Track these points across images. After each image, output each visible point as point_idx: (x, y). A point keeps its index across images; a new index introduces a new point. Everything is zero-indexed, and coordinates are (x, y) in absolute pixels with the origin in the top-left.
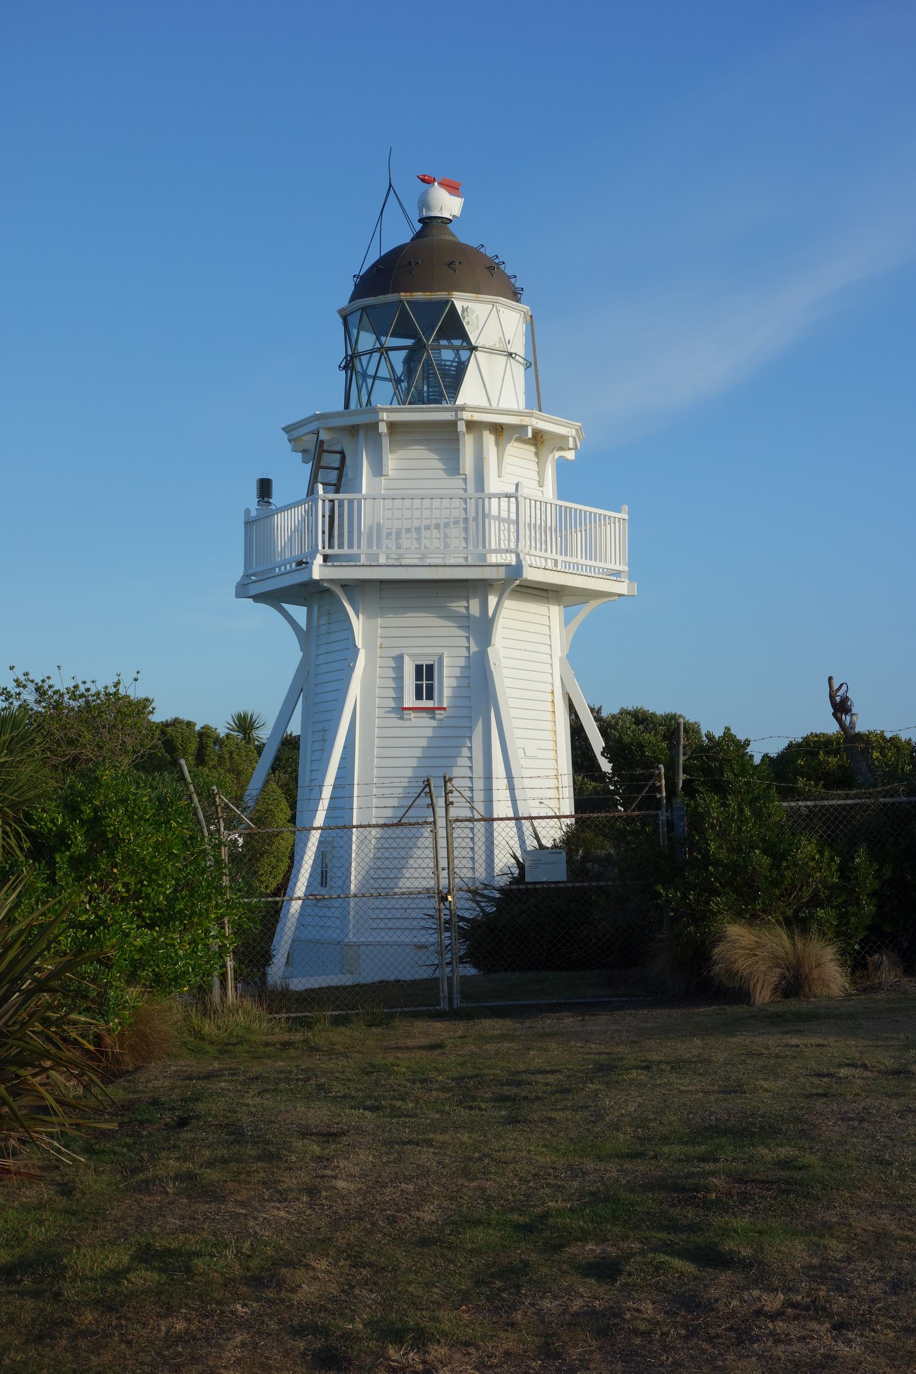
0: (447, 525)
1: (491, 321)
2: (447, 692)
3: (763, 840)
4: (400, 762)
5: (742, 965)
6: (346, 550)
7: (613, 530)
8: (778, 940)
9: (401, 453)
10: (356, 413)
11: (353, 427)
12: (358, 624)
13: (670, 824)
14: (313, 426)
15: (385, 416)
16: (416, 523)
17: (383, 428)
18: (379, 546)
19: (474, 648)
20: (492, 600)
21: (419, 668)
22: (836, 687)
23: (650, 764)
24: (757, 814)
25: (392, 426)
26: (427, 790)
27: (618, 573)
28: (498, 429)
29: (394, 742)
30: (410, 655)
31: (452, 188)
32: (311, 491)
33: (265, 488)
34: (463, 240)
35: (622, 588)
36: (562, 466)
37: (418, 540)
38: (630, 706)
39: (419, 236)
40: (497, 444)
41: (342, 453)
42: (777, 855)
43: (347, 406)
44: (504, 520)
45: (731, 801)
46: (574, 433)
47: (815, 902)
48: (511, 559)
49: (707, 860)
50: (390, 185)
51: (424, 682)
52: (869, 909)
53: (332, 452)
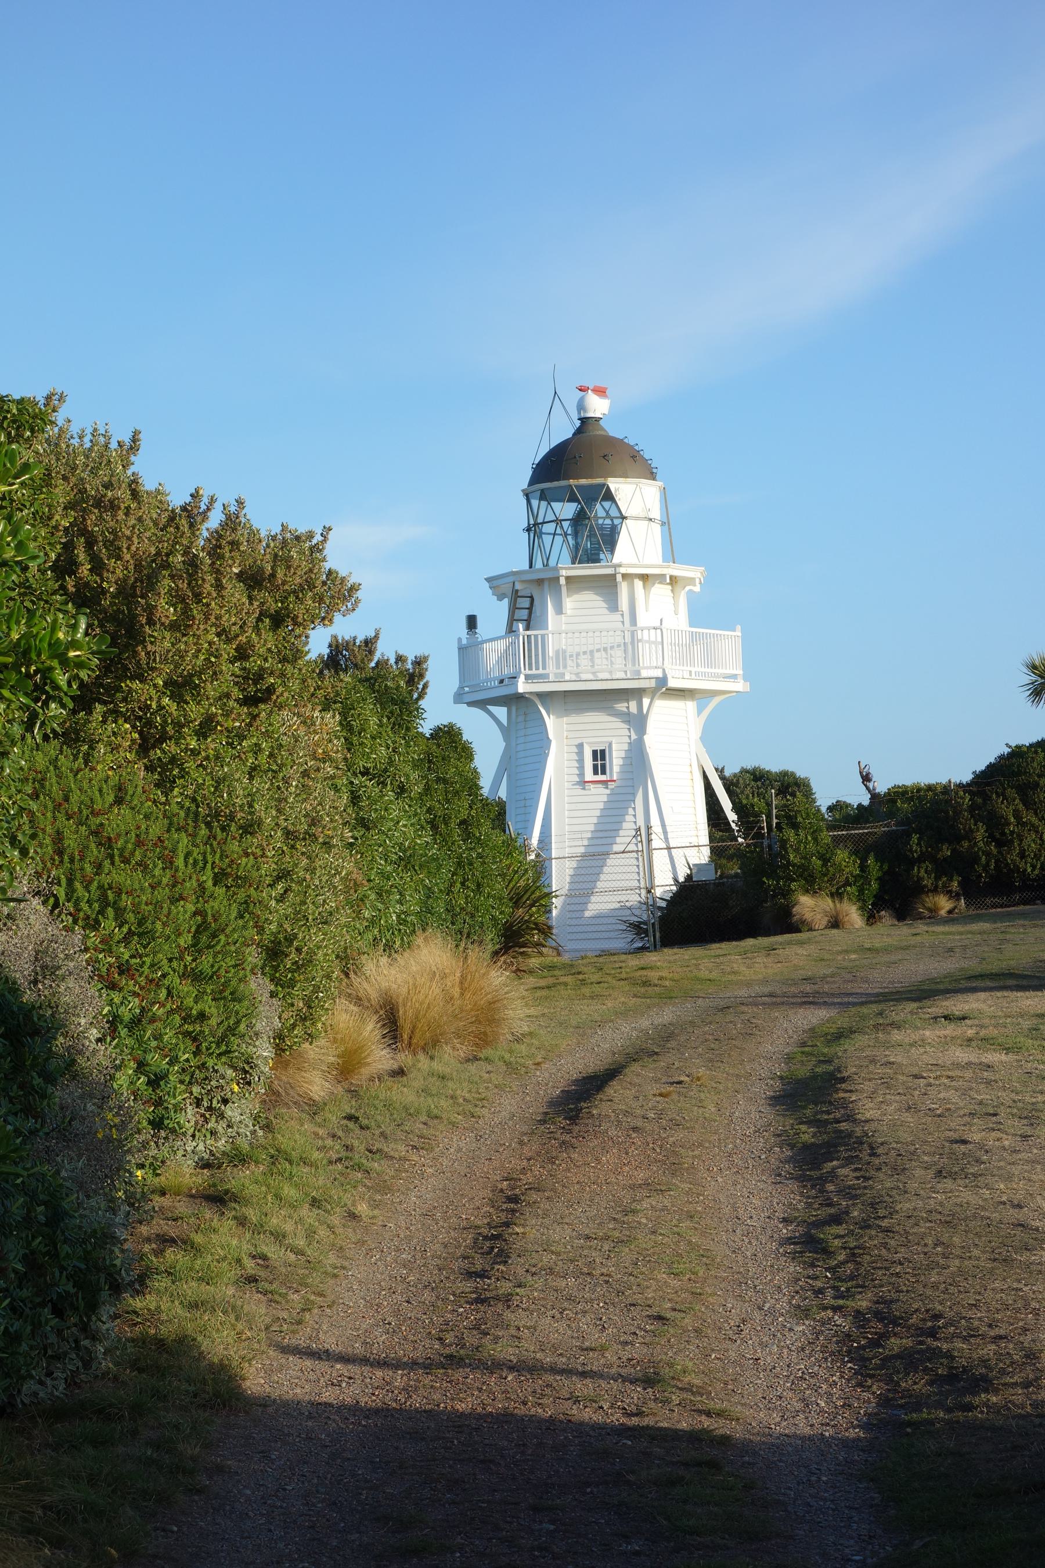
0: (612, 648)
1: (633, 496)
2: (616, 769)
3: (818, 852)
4: (584, 821)
5: (808, 916)
6: (541, 671)
7: (729, 644)
8: (827, 903)
9: (576, 597)
10: (539, 570)
12: (551, 722)
13: (770, 847)
14: (511, 579)
15: (564, 573)
16: (591, 648)
17: (562, 581)
18: (565, 667)
19: (634, 737)
20: (646, 701)
21: (595, 752)
22: (862, 767)
23: (758, 815)
24: (815, 839)
25: (568, 579)
27: (734, 677)
28: (644, 578)
29: (580, 806)
30: (588, 743)
31: (601, 392)
32: (511, 630)
33: (472, 622)
34: (611, 434)
35: (739, 686)
36: (691, 596)
37: (592, 660)
38: (749, 765)
39: (579, 431)
40: (644, 587)
41: (532, 597)
42: (825, 860)
43: (531, 566)
44: (653, 642)
45: (802, 833)
46: (699, 575)
47: (847, 883)
48: (659, 673)
49: (789, 863)
52: (874, 885)
53: (524, 601)
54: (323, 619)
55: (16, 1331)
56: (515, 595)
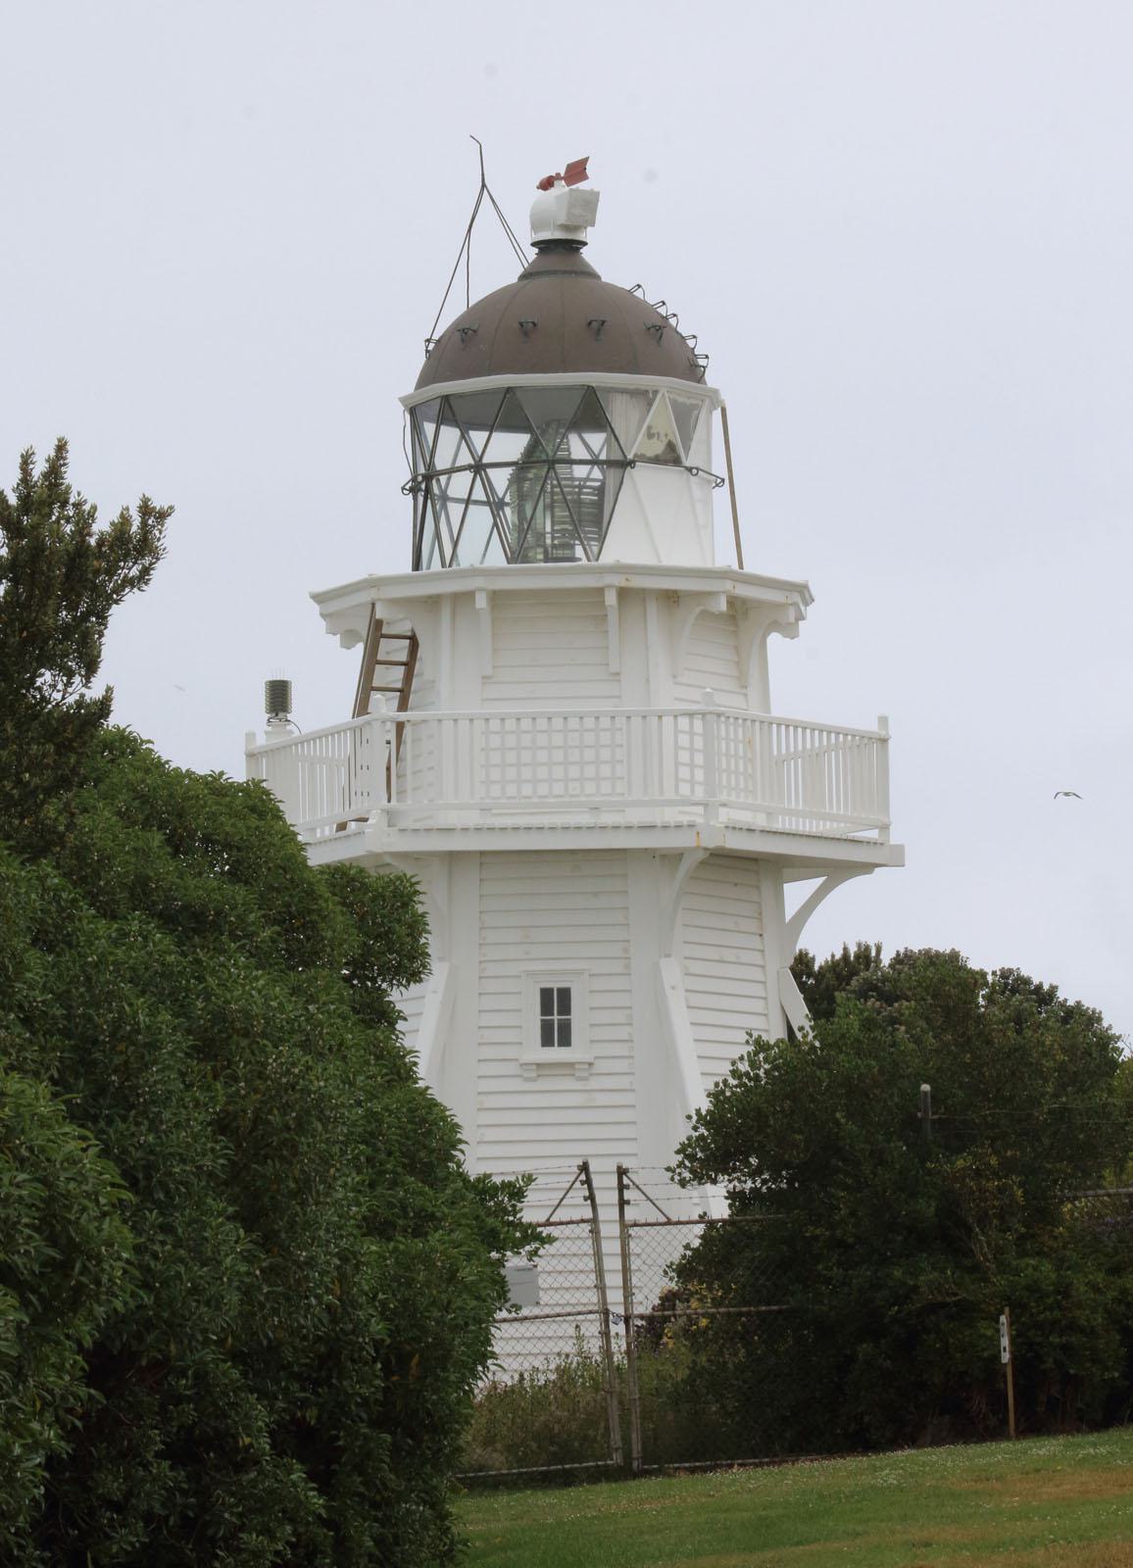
10: (437, 576)
11: (430, 597)
26: (583, 1177)
32: (362, 707)
33: (279, 696)
43: (417, 565)
50: (484, 186)
51: (556, 1017)
54: (64, 748)
55: (447, 1511)
56: (377, 632)
